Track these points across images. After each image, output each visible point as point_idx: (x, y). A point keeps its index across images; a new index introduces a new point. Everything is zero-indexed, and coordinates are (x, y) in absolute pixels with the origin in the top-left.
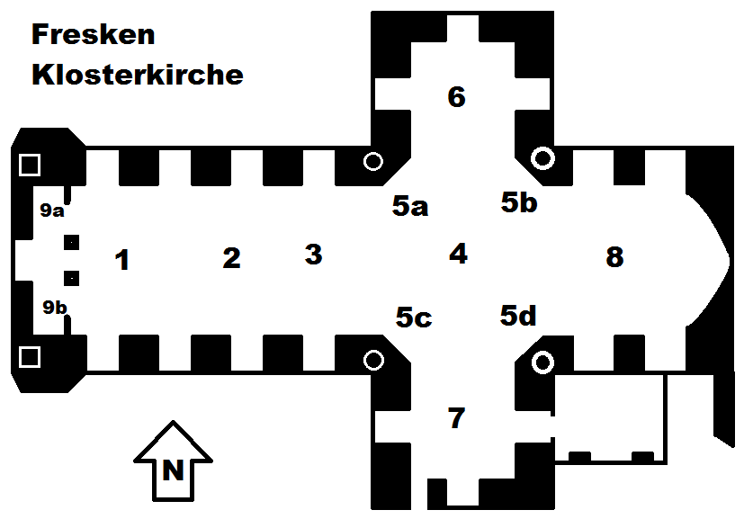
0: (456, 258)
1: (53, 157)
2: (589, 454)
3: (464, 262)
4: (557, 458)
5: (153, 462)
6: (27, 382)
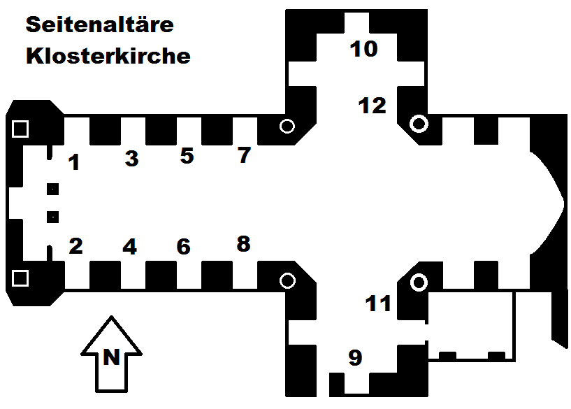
0: (128, 250)
1: (39, 122)
2: (455, 353)
3: (358, 204)
4: (430, 357)
5: (96, 355)
6: (18, 298)
